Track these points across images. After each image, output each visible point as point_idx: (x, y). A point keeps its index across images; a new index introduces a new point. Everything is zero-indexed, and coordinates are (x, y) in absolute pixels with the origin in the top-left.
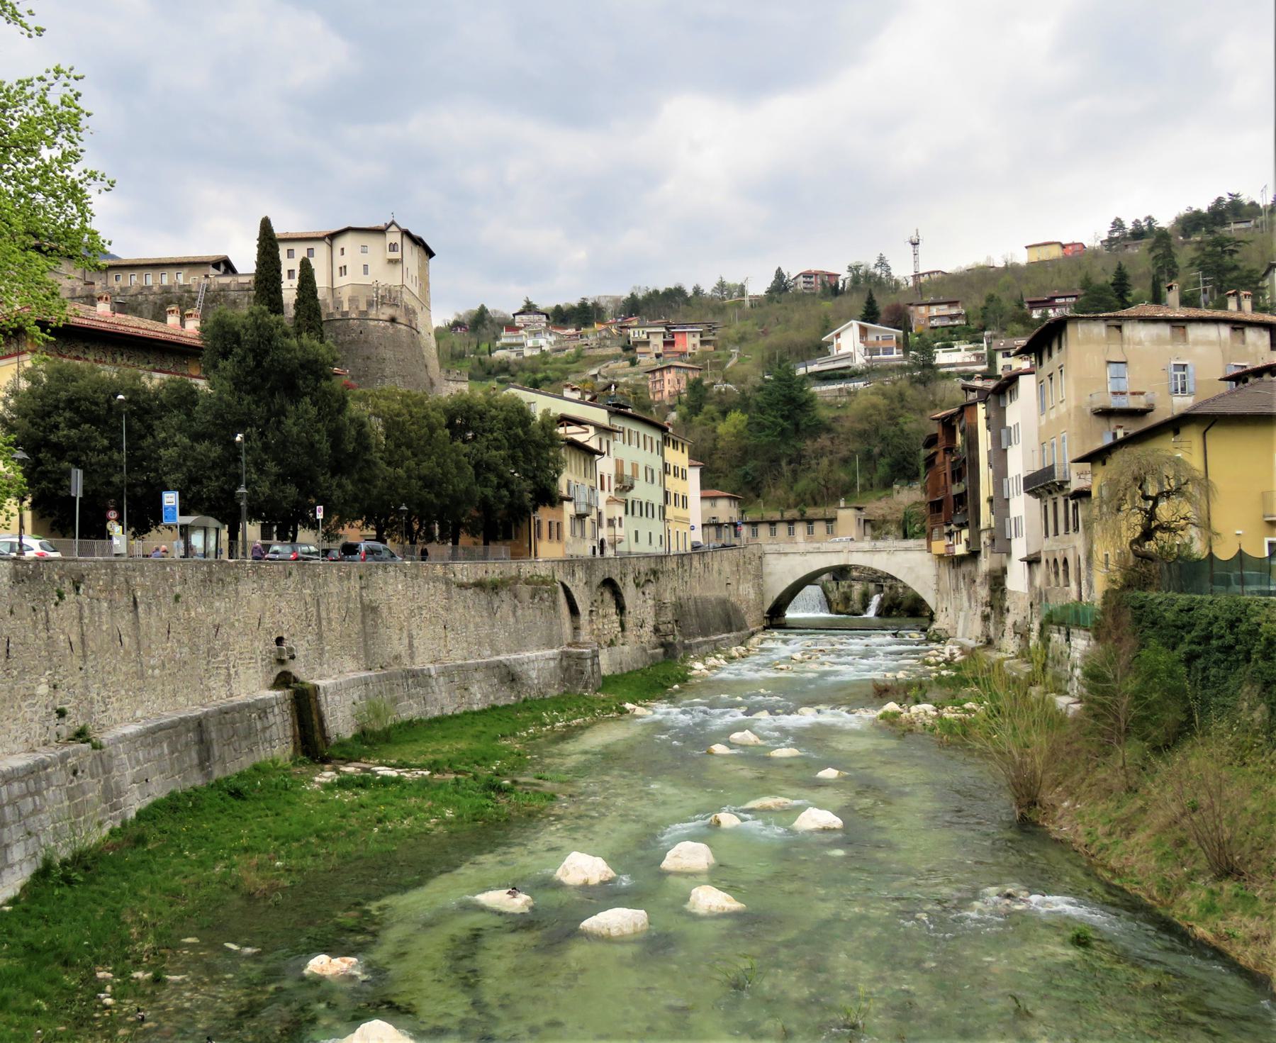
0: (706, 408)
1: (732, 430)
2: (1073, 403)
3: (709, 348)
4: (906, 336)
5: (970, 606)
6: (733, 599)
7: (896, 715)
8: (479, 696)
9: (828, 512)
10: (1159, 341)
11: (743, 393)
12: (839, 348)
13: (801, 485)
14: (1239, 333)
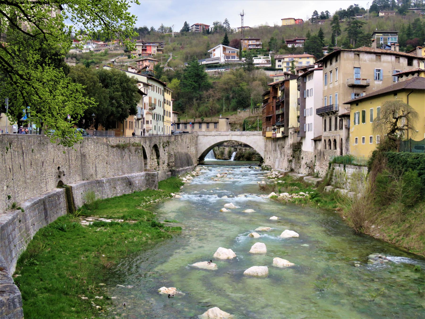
2: (341, 82)
3: (160, 53)
5: (281, 157)
6: (189, 153)
8: (119, 190)
9: (214, 119)
10: (371, 60)
13: (201, 109)
14: (398, 59)
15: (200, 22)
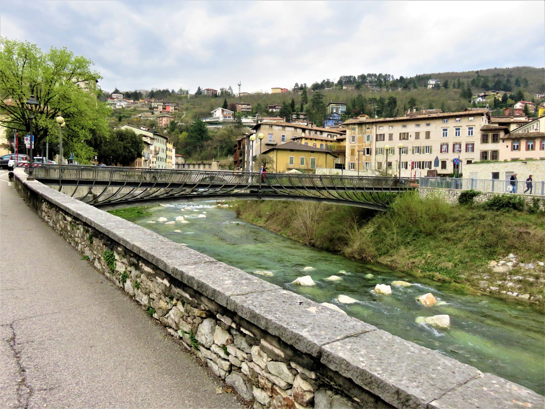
0: (176, 130)
1: (183, 137)
3: (177, 111)
4: (234, 113)
7: (220, 206)
10: (279, 130)
11: (187, 126)
12: (215, 115)
13: (202, 154)
15: (210, 88)
